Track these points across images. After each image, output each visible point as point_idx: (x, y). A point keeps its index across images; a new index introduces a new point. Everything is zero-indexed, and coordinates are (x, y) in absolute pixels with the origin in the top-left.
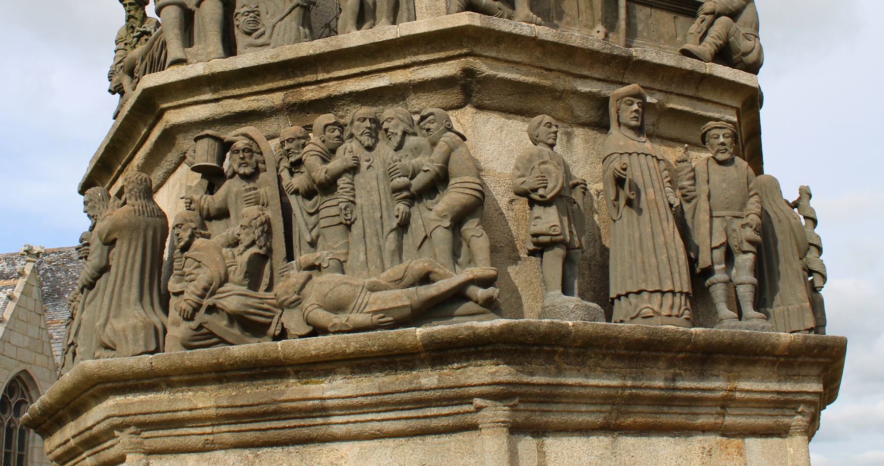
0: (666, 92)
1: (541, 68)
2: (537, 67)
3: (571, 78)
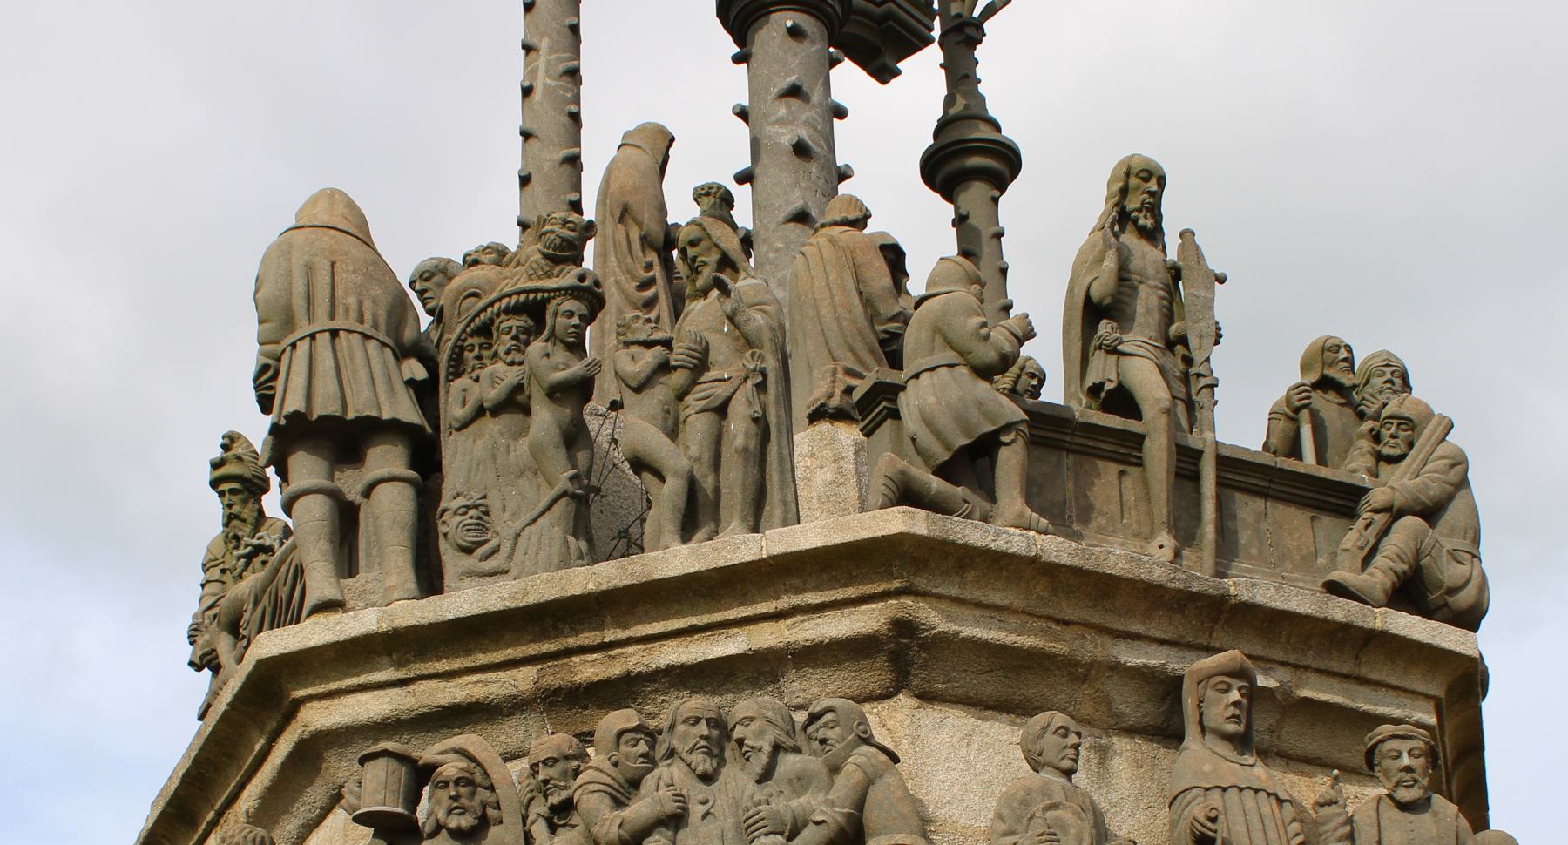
0: (1296, 667)
1: (1049, 618)
2: (1040, 617)
3: (1106, 639)
